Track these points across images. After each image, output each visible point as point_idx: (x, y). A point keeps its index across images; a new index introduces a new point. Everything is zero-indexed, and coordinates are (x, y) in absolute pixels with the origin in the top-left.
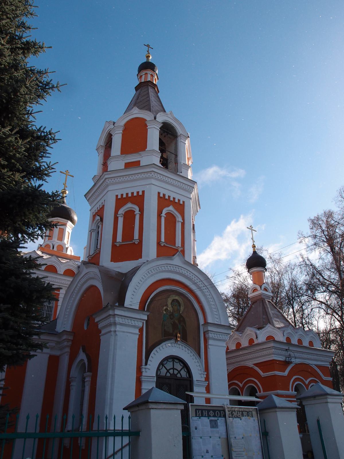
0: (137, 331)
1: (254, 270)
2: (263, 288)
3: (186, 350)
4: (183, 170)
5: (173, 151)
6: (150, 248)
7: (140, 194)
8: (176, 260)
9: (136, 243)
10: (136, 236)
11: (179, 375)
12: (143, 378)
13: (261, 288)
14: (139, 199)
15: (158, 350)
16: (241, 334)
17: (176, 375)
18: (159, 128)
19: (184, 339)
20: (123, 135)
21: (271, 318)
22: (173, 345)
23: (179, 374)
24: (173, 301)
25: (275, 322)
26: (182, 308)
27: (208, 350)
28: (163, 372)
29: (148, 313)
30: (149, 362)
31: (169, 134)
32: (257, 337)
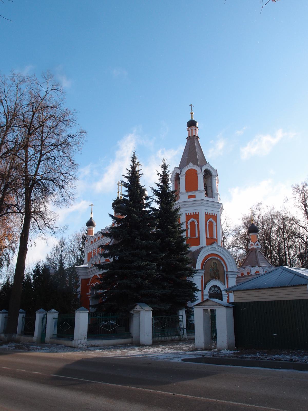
0: (201, 277)
1: (251, 234)
2: (256, 245)
3: (221, 283)
4: (215, 196)
5: (210, 186)
6: (203, 242)
7: (197, 213)
8: (214, 246)
9: (197, 238)
10: (197, 235)
11: (217, 293)
12: (204, 295)
13: (255, 244)
14: (196, 216)
15: (209, 284)
16: (244, 269)
17: (216, 293)
18: (203, 176)
19: (219, 278)
20: (185, 178)
21: (259, 261)
22: (214, 281)
23: (215, 291)
24: (214, 263)
25: (261, 263)
26: (217, 265)
27: (228, 282)
28: (211, 292)
29: (205, 270)
30: (206, 289)
31: (208, 174)
32: (251, 272)
